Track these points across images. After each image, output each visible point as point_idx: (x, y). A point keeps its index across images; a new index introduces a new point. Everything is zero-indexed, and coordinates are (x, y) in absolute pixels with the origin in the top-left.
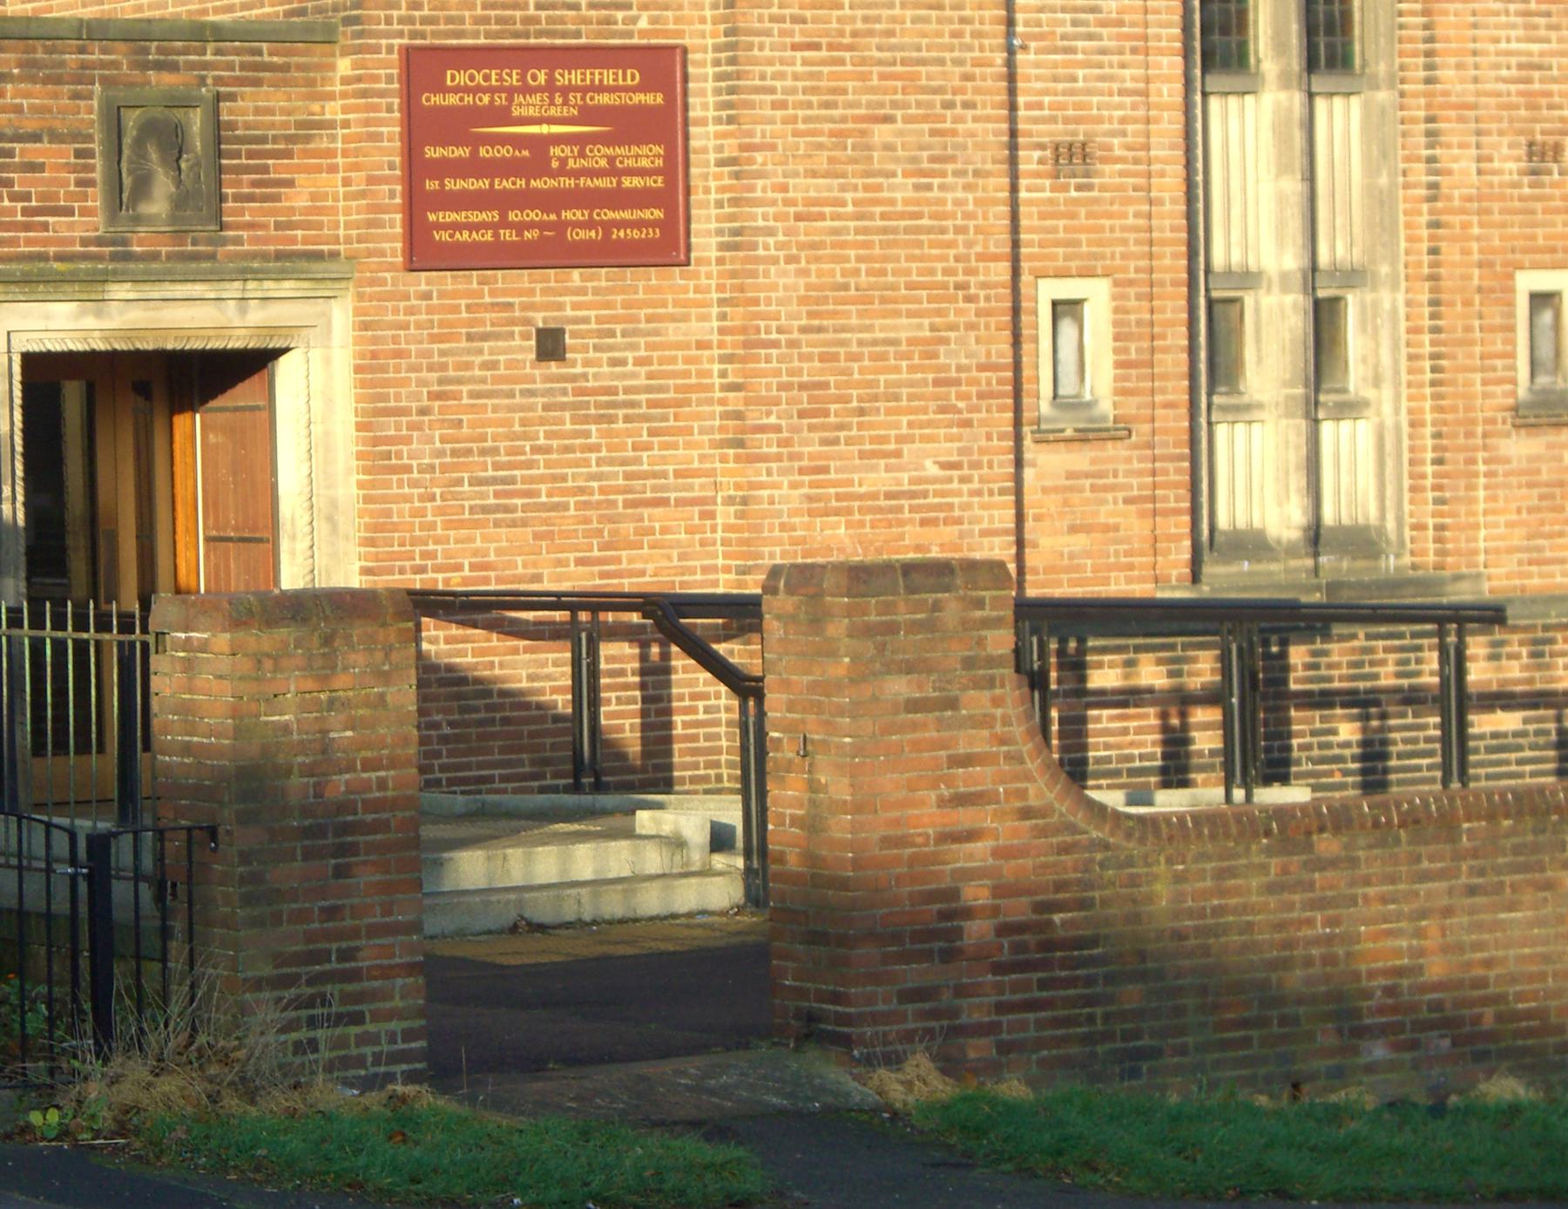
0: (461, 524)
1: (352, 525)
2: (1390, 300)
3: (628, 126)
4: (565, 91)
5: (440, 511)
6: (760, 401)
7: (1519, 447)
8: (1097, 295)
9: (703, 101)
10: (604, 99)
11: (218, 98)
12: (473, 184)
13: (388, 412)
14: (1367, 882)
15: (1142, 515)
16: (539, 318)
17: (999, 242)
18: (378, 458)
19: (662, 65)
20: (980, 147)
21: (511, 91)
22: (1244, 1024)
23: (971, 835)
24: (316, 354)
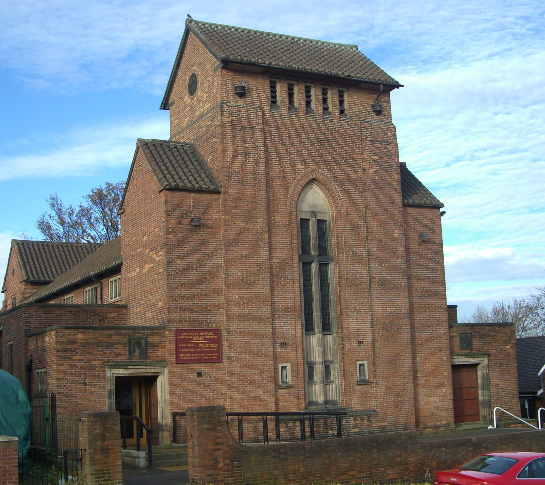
0: (185, 402)
1: (168, 403)
2: (337, 366)
3: (211, 341)
4: (201, 336)
5: (182, 400)
6: (233, 383)
7: (358, 388)
8: (289, 366)
9: (224, 337)
10: (208, 337)
11: (147, 337)
12: (186, 350)
13: (173, 385)
14: (289, 456)
15: (296, 399)
16: (198, 371)
17: (272, 358)
18: (172, 392)
19: (217, 332)
20: (268, 343)
21: (193, 336)
22: (268, 479)
23: (219, 450)
24: (163, 376)
